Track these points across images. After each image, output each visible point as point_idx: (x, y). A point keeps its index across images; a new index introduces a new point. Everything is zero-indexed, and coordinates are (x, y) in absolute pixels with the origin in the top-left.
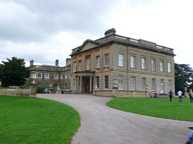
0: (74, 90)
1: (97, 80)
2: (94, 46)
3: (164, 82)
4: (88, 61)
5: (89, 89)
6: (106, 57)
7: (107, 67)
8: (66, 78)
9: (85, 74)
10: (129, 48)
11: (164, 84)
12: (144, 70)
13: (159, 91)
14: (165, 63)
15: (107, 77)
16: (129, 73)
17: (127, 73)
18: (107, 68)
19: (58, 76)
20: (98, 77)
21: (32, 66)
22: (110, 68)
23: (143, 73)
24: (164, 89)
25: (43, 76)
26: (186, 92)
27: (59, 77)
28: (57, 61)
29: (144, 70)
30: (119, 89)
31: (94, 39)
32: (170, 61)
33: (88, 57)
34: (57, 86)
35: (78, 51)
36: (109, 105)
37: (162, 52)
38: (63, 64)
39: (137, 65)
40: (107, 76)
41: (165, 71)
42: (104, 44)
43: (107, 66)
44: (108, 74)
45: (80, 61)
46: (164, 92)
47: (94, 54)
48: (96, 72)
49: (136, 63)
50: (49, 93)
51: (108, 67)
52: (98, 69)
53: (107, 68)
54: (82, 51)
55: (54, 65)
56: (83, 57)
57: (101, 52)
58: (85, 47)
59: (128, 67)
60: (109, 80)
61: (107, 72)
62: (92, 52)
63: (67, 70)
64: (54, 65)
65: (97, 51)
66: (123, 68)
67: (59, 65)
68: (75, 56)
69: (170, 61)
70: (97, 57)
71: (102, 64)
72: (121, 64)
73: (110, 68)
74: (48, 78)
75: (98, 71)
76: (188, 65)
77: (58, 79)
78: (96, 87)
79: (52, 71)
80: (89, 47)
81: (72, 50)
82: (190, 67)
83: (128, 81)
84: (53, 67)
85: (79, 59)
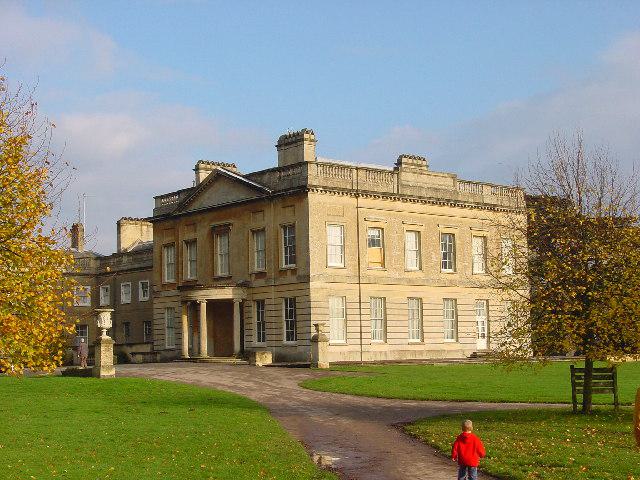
0: (167, 347)
2: (242, 195)
4: (221, 245)
5: (232, 344)
7: (289, 269)
10: (362, 200)
18: (289, 273)
20: (261, 304)
30: (331, 342)
33: (222, 231)
35: (181, 206)
37: (420, 244)
40: (291, 299)
42: (279, 191)
43: (289, 265)
44: (296, 293)
51: (294, 271)
52: (260, 275)
53: (289, 273)
54: (196, 206)
58: (207, 195)
59: (131, 270)
60: (298, 312)
63: (130, 267)
66: (344, 272)
68: (168, 224)
75: (261, 282)
78: (255, 338)
81: (156, 198)
83: (361, 333)
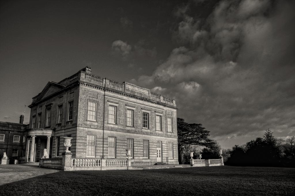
1: (58, 142)
2: (56, 90)
3: (162, 146)
6: (70, 106)
11: (162, 148)
12: (131, 127)
13: (154, 158)
14: (163, 118)
16: (105, 96)
17: (101, 131)
19: (4, 136)
22: (74, 122)
23: (128, 131)
24: (162, 155)
26: (192, 159)
27: (21, 140)
29: (131, 127)
31: (57, 81)
32: (170, 116)
34: (280, 155)
39: (120, 119)
41: (174, 131)
45: (40, 114)
46: (162, 159)
48: (56, 130)
49: (118, 117)
52: (59, 125)
57: (66, 98)
61: (70, 130)
62: (54, 100)
65: (60, 98)
69: (170, 116)
70: (60, 106)
71: (65, 116)
73: (74, 122)
74: (3, 141)
76: (200, 124)
77: (19, 142)
79: (11, 131)
80: (52, 91)
81: (33, 98)
82: (202, 127)
85: (39, 110)
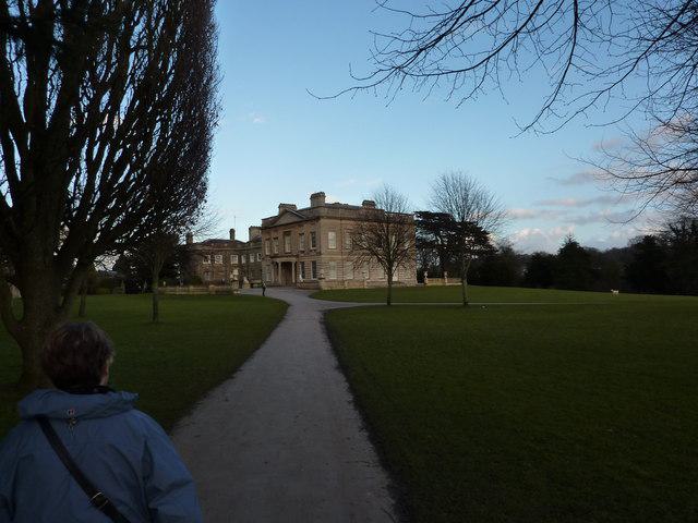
4: (287, 238)
8: (252, 261)
9: (284, 260)
15: (314, 263)
21: (190, 243)
25: (213, 261)
27: (240, 260)
28: (349, 402)
33: (287, 234)
36: (310, 297)
38: (243, 236)
47: (296, 231)
50: (137, 291)
55: (228, 237)
56: (280, 234)
57: (307, 228)
64: (228, 237)
67: (236, 238)
72: (332, 245)
84: (226, 241)
